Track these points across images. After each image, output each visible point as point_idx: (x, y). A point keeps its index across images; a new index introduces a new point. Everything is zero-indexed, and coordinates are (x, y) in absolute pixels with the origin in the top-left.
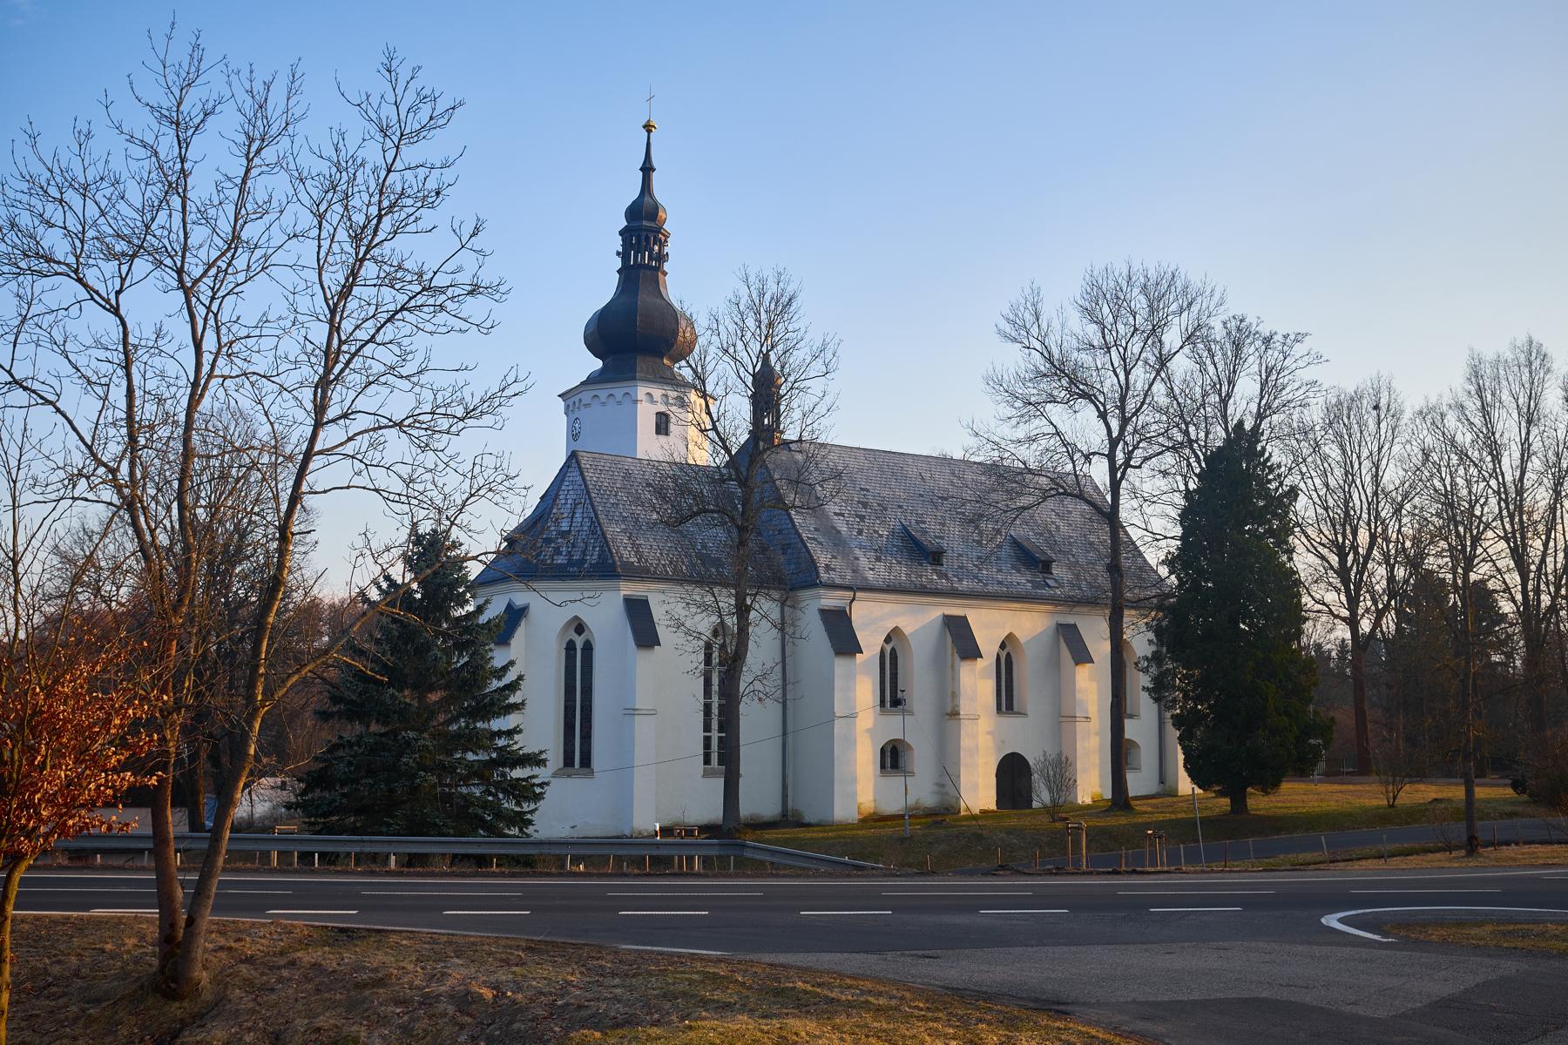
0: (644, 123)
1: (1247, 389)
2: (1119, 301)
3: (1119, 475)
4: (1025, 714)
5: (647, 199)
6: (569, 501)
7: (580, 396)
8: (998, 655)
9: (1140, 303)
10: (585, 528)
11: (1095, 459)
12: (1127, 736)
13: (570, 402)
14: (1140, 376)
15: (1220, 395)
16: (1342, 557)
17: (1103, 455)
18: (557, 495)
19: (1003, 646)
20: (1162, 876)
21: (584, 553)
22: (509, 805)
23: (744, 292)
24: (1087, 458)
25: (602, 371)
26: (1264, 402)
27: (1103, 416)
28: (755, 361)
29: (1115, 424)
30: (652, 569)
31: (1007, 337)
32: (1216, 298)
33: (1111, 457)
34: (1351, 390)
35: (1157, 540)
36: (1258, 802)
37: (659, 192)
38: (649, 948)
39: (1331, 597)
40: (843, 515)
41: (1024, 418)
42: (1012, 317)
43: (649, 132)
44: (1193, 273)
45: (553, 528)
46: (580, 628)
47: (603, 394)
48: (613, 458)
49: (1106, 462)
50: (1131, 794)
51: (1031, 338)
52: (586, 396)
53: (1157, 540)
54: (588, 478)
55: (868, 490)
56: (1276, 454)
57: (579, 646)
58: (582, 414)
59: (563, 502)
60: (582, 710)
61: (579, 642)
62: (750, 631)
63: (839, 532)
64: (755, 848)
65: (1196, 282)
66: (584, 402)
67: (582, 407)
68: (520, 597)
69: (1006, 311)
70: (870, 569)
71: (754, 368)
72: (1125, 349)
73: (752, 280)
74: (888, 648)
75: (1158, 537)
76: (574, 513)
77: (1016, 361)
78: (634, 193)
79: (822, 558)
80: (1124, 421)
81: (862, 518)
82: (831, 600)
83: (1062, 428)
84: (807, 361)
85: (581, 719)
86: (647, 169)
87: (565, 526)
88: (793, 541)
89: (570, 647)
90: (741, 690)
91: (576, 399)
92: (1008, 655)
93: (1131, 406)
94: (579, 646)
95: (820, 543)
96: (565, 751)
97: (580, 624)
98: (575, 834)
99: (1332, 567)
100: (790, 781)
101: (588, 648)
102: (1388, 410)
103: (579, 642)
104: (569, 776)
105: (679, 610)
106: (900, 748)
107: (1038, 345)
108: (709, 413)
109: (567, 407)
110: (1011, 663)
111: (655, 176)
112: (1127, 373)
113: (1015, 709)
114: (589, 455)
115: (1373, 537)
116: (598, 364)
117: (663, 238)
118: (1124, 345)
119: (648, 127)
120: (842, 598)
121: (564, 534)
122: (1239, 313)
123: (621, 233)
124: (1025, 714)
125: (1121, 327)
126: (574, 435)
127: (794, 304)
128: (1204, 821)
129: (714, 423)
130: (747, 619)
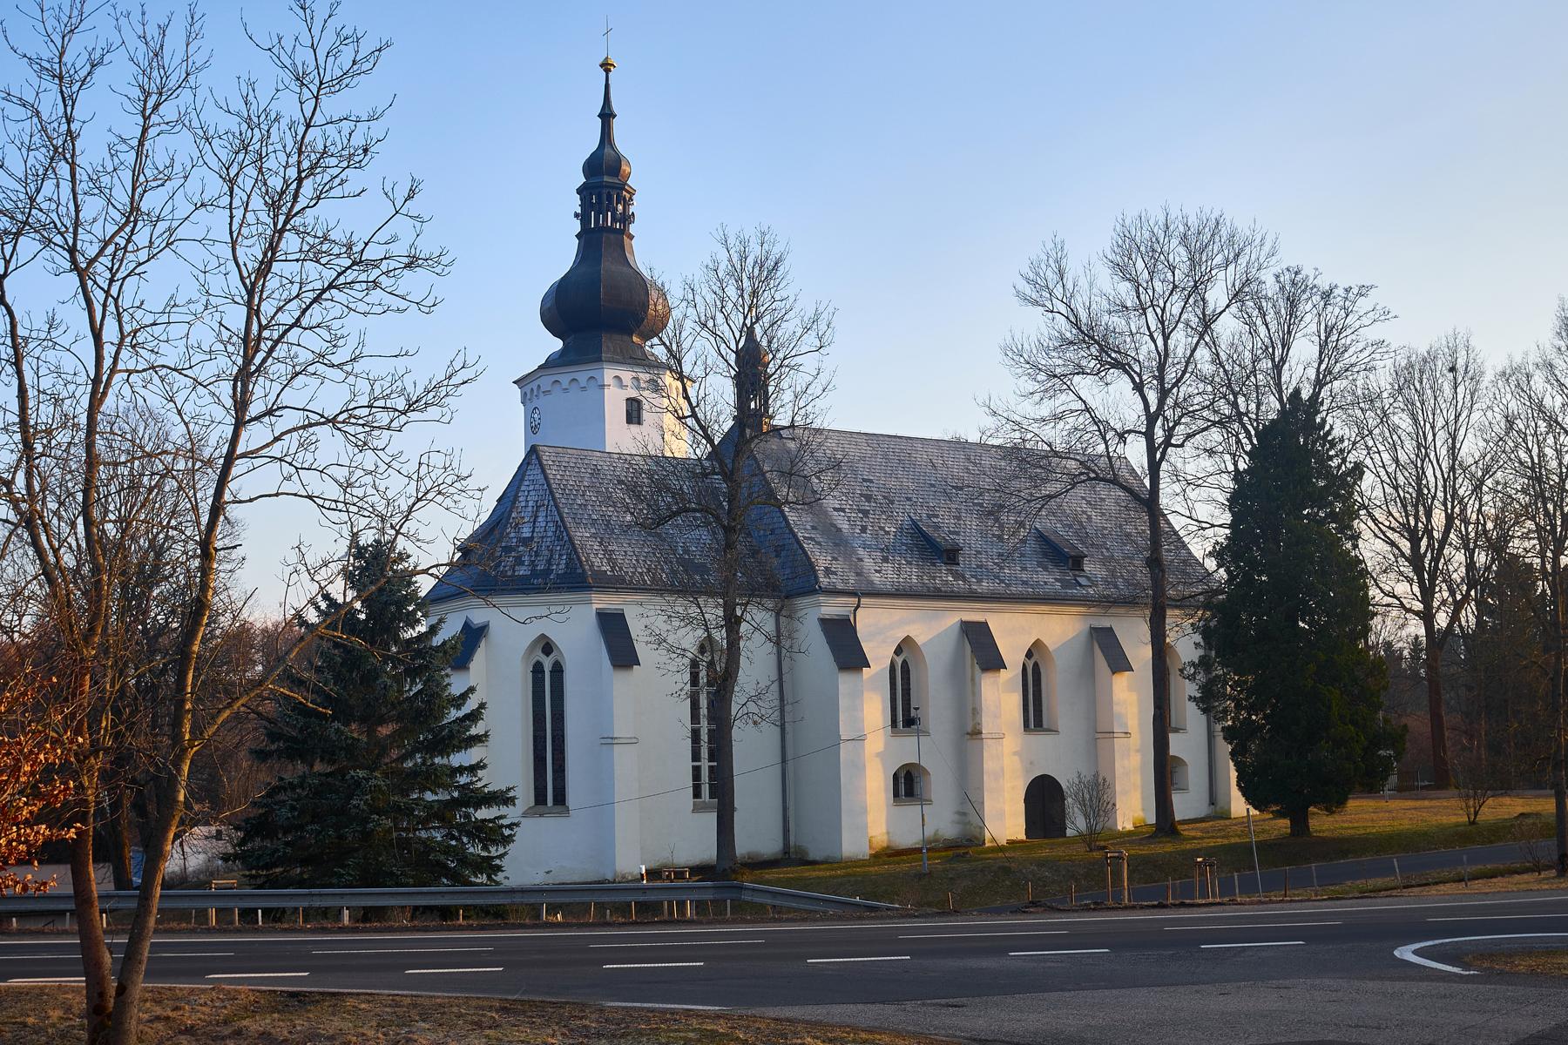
0: (601, 61)
1: (1304, 351)
3: (1158, 456)
5: (607, 150)
6: (531, 504)
8: (1024, 664)
10: (550, 534)
11: (1130, 438)
13: (528, 389)
14: (1180, 341)
16: (1415, 542)
17: (1140, 432)
18: (516, 497)
19: (1029, 654)
21: (549, 562)
22: (475, 849)
24: (1122, 437)
25: (563, 352)
26: (1323, 367)
29: (1152, 397)
33: (1149, 435)
34: (1423, 350)
35: (1204, 529)
36: (1322, 823)
40: (843, 510)
42: (1032, 276)
43: (607, 71)
45: (512, 535)
47: (565, 379)
50: (1177, 818)
51: (1054, 300)
52: (545, 382)
53: (1204, 529)
54: (551, 476)
55: (871, 481)
56: (1338, 426)
58: (541, 402)
59: (523, 504)
60: (553, 741)
61: (548, 664)
65: (1244, 230)
67: (541, 395)
68: (479, 616)
69: (1026, 270)
70: (876, 571)
72: (1163, 310)
74: (899, 661)
75: (1204, 525)
76: (536, 517)
80: (1164, 394)
81: (866, 513)
82: (833, 607)
83: (1092, 403)
84: (798, 335)
86: (607, 115)
87: (526, 532)
89: (538, 669)
90: (733, 713)
91: (534, 385)
92: (1036, 665)
95: (819, 543)
97: (547, 644)
98: (550, 880)
99: (1403, 555)
100: (791, 813)
101: (558, 670)
102: (1466, 372)
103: (548, 664)
104: (541, 815)
106: (915, 773)
107: (1062, 308)
108: (687, 398)
109: (524, 395)
111: (616, 123)
112: (1166, 338)
113: (1045, 726)
115: (1450, 519)
116: (558, 344)
117: (628, 196)
119: (606, 66)
120: (845, 605)
121: (526, 542)
122: (1293, 264)
123: (579, 191)
125: (1158, 285)
126: (532, 427)
127: (781, 269)
129: (693, 409)
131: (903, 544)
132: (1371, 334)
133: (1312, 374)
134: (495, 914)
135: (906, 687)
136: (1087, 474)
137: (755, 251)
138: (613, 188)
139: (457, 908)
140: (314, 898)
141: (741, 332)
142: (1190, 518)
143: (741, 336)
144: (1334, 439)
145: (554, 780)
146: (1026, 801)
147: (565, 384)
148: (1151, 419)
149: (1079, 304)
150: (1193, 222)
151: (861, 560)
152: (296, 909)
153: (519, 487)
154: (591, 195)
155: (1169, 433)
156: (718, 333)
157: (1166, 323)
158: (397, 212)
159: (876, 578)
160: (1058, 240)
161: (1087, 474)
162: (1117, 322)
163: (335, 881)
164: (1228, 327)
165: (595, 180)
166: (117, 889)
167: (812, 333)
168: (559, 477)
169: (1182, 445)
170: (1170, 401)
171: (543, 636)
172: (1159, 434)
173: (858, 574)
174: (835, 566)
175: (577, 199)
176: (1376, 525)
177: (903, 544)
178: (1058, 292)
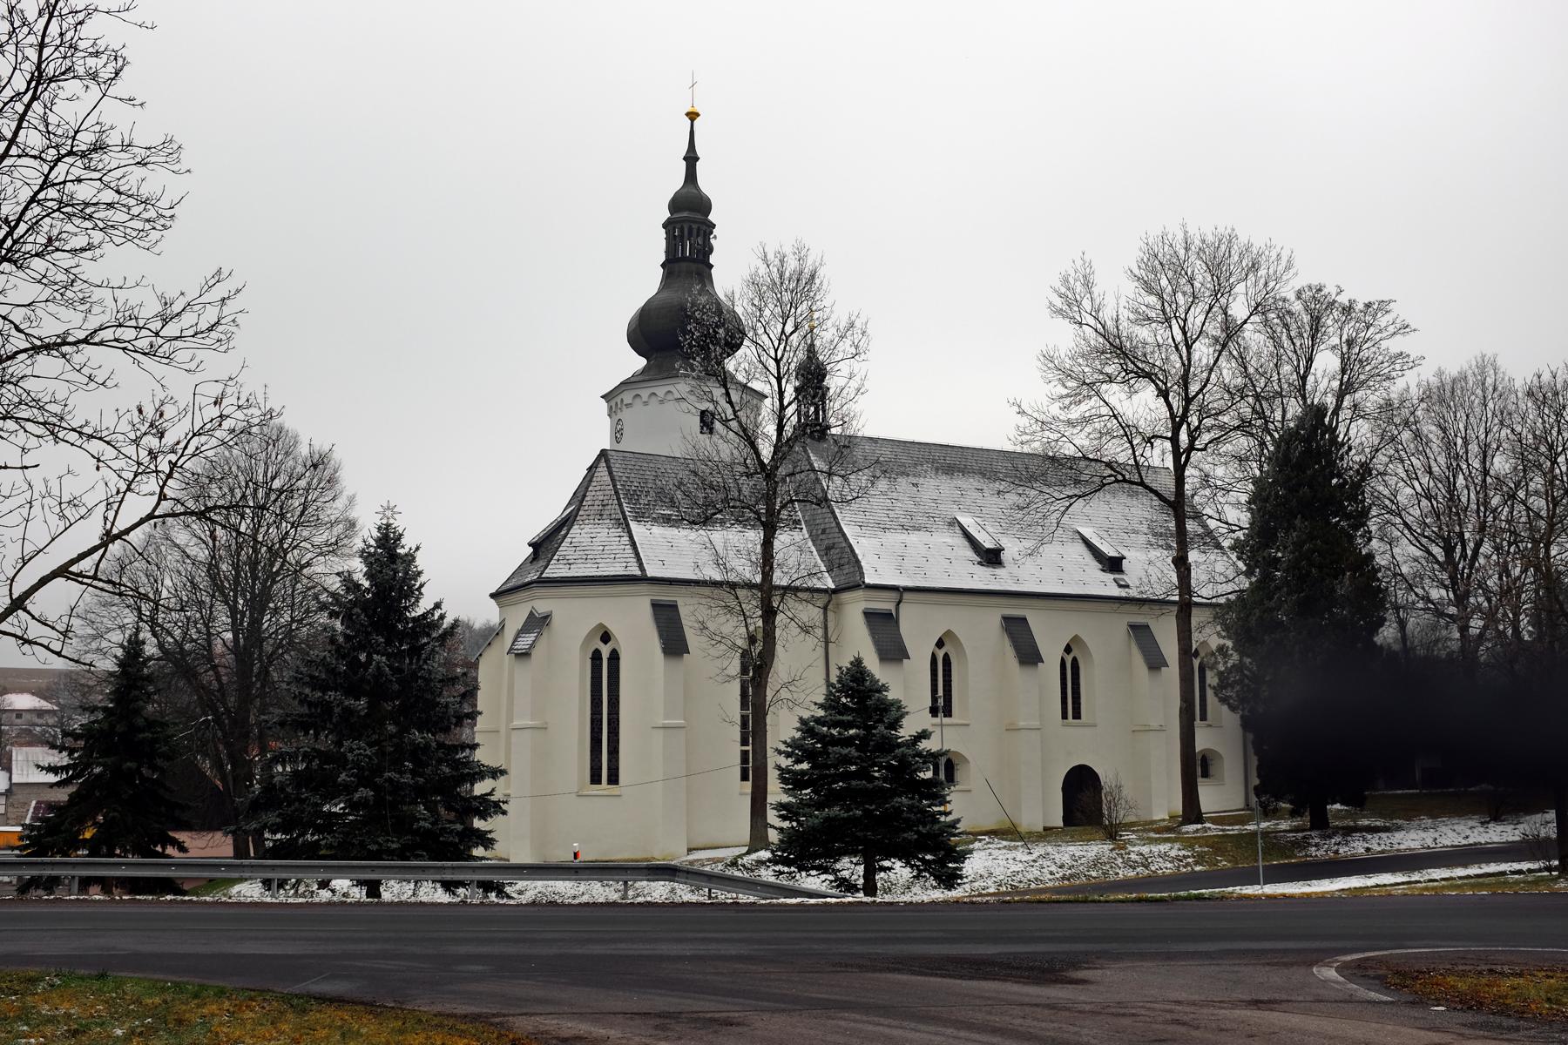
1: (1326, 363)
2: (1179, 269)
3: (1183, 459)
4: (492, 596)
8: (1062, 659)
9: (1202, 277)
11: (1157, 442)
14: (1203, 352)
15: (1298, 373)
16: (1449, 550)
17: (1166, 438)
18: (584, 496)
23: (763, 270)
24: (1149, 441)
25: (645, 370)
26: (1346, 377)
27: (1164, 394)
28: (776, 344)
29: (1176, 403)
31: (1060, 312)
32: (1284, 263)
33: (1174, 440)
34: (1455, 373)
35: (1234, 531)
37: (705, 183)
39: (1436, 594)
41: (1076, 398)
42: (1063, 290)
43: (692, 121)
44: (1253, 233)
46: (606, 637)
47: (645, 394)
48: (645, 457)
49: (1168, 445)
50: (1203, 811)
51: (1083, 313)
52: (627, 397)
53: (1234, 531)
54: (617, 478)
56: (1359, 434)
58: (625, 415)
60: (609, 724)
61: (605, 651)
62: (777, 635)
65: (1258, 243)
68: (542, 607)
69: (1057, 284)
71: (776, 351)
72: (1185, 320)
73: (771, 256)
74: (940, 654)
75: (1234, 528)
77: (1066, 339)
78: (678, 181)
80: (1188, 401)
82: (884, 604)
83: (1119, 409)
84: (835, 342)
86: (691, 159)
88: (836, 540)
89: (596, 656)
90: (768, 698)
91: (618, 399)
92: (1075, 661)
93: (1194, 388)
96: (592, 768)
97: (606, 632)
99: (1437, 562)
101: (615, 657)
102: (1495, 389)
103: (605, 651)
105: (703, 613)
106: (955, 761)
107: (1092, 321)
108: (730, 402)
109: (610, 408)
110: (1078, 668)
112: (1189, 347)
114: (618, 454)
115: (1482, 528)
118: (1183, 316)
119: (693, 116)
122: (1315, 282)
123: (665, 226)
124: (492, 596)
125: (1180, 298)
126: (618, 434)
127: (817, 281)
128: (742, 764)
129: (735, 412)
130: (774, 622)
132: (1394, 345)
133: (1335, 384)
135: (947, 678)
136: (1115, 476)
137: (791, 265)
140: (245, 869)
141: (779, 340)
142: (1220, 520)
143: (779, 344)
145: (609, 761)
146: (1063, 789)
147: (645, 398)
148: (1177, 422)
149: (1107, 315)
150: (1210, 238)
152: (73, 877)
153: (587, 488)
155: (1192, 439)
156: (759, 342)
157: (1189, 335)
158: (104, 95)
160: (1087, 258)
161: (1115, 476)
162: (1144, 333)
164: (1254, 338)
166: (236, 857)
167: (848, 342)
168: (624, 479)
169: (1204, 449)
170: (1193, 407)
171: (601, 626)
172: (1184, 437)
175: (662, 233)
176: (1412, 534)
178: (1086, 304)
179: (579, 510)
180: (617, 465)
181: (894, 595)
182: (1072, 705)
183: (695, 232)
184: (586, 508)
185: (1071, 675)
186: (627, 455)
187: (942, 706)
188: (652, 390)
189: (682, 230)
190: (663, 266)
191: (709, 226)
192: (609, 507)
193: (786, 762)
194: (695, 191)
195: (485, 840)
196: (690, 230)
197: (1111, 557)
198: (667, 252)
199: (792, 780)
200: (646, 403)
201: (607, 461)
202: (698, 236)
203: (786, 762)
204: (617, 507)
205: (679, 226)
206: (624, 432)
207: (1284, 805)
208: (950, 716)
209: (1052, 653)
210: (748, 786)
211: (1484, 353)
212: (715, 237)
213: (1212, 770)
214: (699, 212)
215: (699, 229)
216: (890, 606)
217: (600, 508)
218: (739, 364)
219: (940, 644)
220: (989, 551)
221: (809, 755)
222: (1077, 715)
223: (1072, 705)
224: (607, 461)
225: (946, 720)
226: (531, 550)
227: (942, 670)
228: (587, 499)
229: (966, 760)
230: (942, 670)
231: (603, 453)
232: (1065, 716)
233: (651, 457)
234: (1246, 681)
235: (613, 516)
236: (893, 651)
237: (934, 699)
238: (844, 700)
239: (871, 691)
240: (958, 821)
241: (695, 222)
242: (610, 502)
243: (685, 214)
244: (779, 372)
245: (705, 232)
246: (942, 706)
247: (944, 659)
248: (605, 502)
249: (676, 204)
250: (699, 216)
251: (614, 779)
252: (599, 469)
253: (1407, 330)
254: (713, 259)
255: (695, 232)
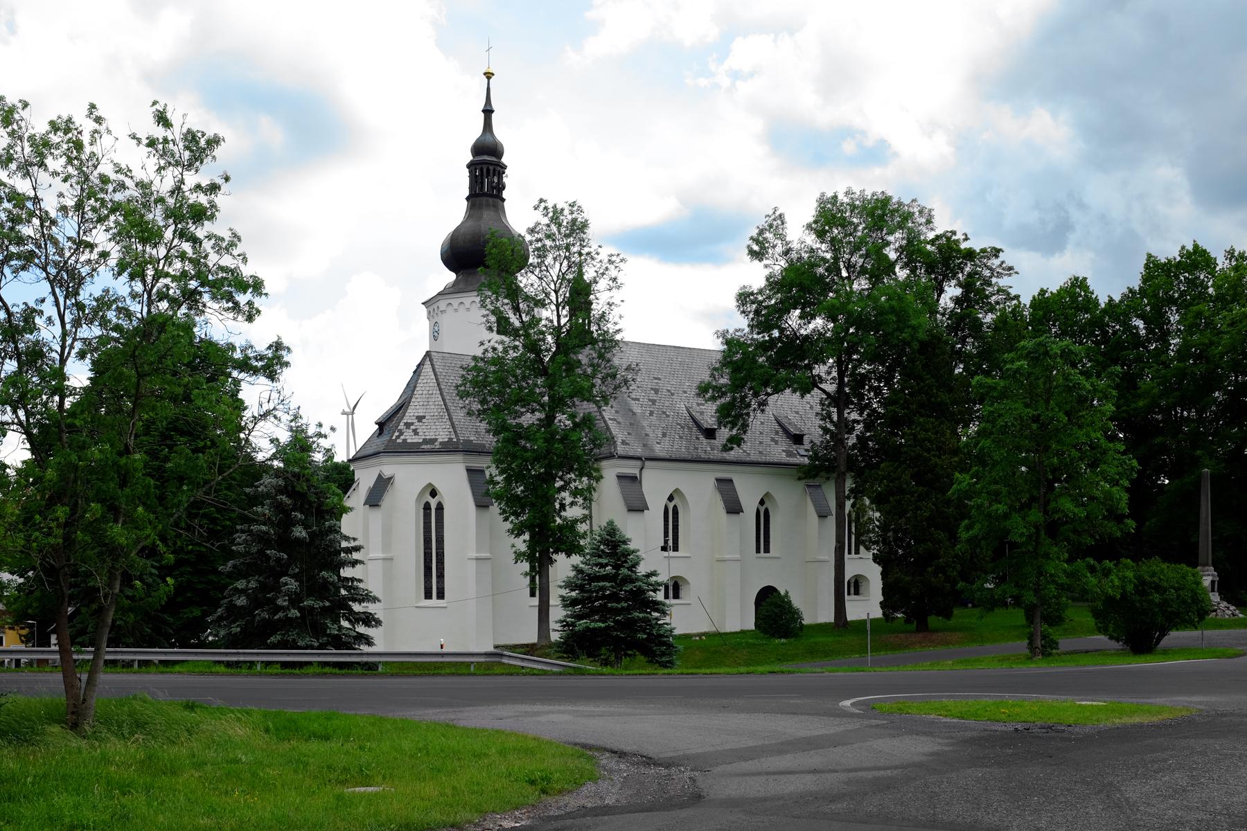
7: (437, 304)
12: (880, 569)
20: (526, 661)
22: (361, 629)
25: (455, 283)
30: (487, 445)
38: (1094, 703)
43: (489, 78)
46: (434, 493)
47: (455, 302)
52: (442, 304)
54: (438, 374)
55: (659, 379)
57: (433, 507)
60: (437, 556)
61: (433, 503)
63: (634, 414)
64: (510, 656)
66: (441, 309)
68: (387, 471)
78: (476, 131)
79: (618, 433)
82: (631, 468)
85: (437, 562)
86: (488, 112)
89: (427, 507)
91: (435, 306)
94: (433, 507)
95: (619, 423)
97: (433, 489)
101: (440, 508)
103: (433, 503)
106: (680, 583)
109: (429, 313)
111: (495, 117)
116: (451, 276)
119: (489, 75)
120: (634, 467)
123: (469, 166)
126: (435, 335)
131: (678, 424)
134: (370, 668)
138: (491, 164)
139: (133, 661)
144: (821, 420)
145: (438, 582)
151: (647, 435)
152: (12, 660)
153: (417, 381)
154: (476, 169)
159: (657, 448)
163: (206, 663)
165: (477, 158)
171: (430, 484)
173: (644, 445)
174: (629, 439)
177: (678, 424)
179: (411, 398)
180: (438, 363)
181: (639, 463)
182: (763, 541)
183: (491, 171)
184: (417, 396)
185: (763, 521)
186: (445, 355)
187: (672, 542)
188: (461, 300)
189: (481, 170)
190: (468, 199)
191: (502, 168)
192: (434, 396)
193: (564, 592)
194: (491, 139)
195: (368, 641)
196: (488, 170)
197: (795, 435)
198: (471, 188)
199: (568, 603)
200: (456, 310)
201: (431, 360)
202: (494, 176)
203: (564, 592)
204: (440, 396)
205: (479, 167)
206: (440, 332)
207: (899, 615)
208: (677, 551)
209: (750, 504)
210: (535, 601)
211: (1077, 276)
212: (507, 176)
213: (862, 590)
214: (494, 156)
215: (494, 170)
216: (636, 472)
217: (427, 396)
218: (527, 281)
219: (671, 498)
220: (707, 429)
221: (581, 588)
222: (767, 550)
223: (763, 541)
224: (431, 360)
225: (675, 554)
226: (377, 427)
227: (672, 519)
228: (417, 389)
229: (688, 583)
230: (672, 519)
231: (428, 354)
232: (758, 551)
233: (462, 357)
234: (877, 529)
235: (437, 403)
236: (637, 506)
237: (666, 542)
238: (602, 547)
239: (620, 541)
240: (674, 629)
241: (491, 164)
242: (434, 392)
243: (486, 158)
244: (557, 301)
245: (499, 172)
246: (672, 542)
247: (673, 510)
248: (430, 392)
249: (478, 149)
250: (494, 159)
251: (441, 595)
252: (425, 366)
253: (1011, 272)
254: (505, 194)
255: (491, 171)
